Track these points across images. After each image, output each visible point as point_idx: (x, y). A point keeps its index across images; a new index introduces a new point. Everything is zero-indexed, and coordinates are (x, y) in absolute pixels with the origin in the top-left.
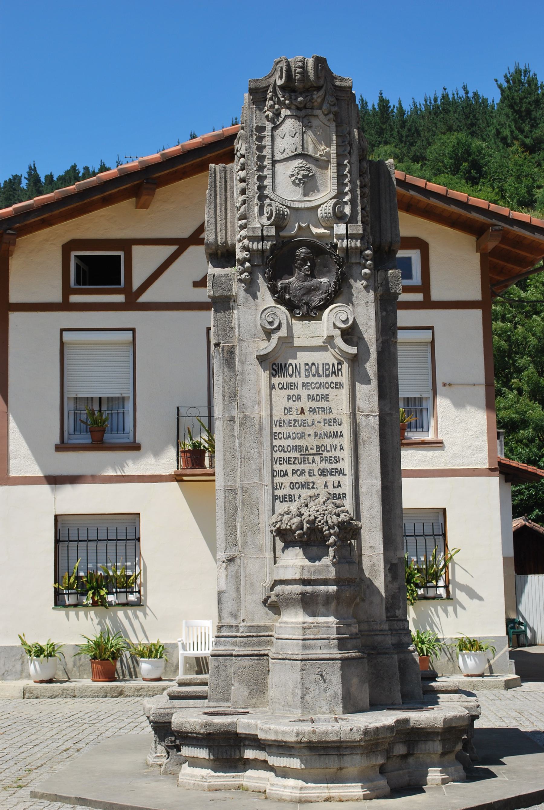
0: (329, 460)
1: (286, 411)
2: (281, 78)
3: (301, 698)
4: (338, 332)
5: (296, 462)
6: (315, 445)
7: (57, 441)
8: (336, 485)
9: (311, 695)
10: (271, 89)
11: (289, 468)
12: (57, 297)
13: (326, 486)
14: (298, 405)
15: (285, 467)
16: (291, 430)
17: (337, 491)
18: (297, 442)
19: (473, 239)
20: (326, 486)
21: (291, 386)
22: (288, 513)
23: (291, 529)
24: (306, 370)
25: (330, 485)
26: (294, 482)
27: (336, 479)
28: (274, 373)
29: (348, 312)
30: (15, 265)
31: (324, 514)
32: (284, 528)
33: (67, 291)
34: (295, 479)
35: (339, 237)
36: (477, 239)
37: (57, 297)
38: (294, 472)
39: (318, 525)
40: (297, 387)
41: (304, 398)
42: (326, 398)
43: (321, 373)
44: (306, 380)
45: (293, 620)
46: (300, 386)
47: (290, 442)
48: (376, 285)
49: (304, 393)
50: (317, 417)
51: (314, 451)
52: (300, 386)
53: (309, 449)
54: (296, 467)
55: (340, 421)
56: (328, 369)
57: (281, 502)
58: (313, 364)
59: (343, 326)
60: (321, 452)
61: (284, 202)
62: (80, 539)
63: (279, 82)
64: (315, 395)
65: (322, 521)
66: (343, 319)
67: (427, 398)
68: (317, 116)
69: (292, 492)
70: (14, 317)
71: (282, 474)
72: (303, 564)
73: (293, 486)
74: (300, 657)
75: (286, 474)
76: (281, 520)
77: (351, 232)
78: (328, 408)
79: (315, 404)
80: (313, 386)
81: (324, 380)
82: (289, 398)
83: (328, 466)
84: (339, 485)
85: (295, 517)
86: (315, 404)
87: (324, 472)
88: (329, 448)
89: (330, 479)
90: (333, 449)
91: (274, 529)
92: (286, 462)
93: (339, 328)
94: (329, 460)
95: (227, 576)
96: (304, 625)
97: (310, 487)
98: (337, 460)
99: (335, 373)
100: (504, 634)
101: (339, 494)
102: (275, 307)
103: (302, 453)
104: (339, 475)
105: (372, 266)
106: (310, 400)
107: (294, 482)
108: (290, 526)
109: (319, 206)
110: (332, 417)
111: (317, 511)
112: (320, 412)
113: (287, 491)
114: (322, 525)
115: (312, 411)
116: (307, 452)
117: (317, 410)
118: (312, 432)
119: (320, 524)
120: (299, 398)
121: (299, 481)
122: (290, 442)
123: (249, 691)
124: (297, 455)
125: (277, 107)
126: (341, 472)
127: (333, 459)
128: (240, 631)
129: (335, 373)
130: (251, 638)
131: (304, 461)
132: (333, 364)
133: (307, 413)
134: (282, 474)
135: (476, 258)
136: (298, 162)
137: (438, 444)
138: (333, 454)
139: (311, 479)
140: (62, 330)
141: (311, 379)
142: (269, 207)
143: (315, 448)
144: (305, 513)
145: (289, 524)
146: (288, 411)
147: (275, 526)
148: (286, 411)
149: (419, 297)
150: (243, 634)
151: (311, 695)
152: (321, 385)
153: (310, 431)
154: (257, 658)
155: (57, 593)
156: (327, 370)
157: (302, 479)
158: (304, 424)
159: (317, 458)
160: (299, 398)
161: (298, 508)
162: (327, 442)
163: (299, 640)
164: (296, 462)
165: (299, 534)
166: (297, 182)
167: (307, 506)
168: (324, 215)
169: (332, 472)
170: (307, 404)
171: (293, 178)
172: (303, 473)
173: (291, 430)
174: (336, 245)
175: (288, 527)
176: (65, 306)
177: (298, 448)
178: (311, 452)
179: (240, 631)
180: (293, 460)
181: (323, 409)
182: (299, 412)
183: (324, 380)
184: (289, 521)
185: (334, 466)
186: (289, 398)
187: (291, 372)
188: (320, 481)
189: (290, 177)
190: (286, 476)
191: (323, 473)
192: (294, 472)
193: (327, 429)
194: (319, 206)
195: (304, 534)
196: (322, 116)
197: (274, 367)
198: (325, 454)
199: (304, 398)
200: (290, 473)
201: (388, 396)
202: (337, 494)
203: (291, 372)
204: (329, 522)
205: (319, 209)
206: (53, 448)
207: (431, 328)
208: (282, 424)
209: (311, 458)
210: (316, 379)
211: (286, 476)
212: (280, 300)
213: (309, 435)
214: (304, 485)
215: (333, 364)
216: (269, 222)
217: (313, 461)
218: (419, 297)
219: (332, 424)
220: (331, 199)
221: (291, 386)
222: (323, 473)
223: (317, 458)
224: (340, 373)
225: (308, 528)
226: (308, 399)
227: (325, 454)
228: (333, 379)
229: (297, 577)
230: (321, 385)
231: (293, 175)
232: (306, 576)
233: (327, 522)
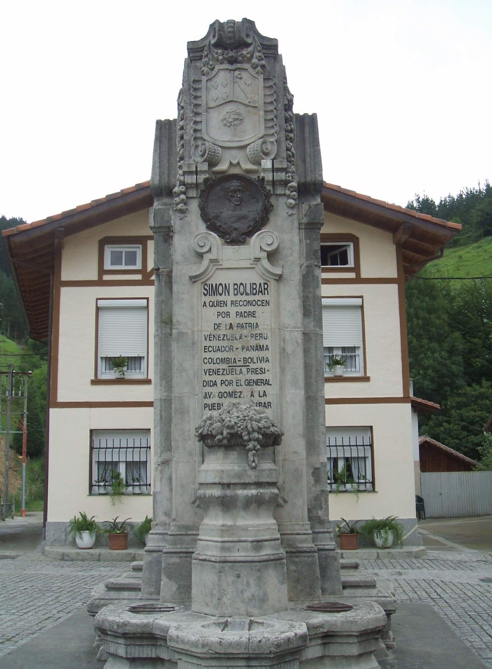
0: (255, 371)
1: (216, 327)
2: (214, 37)
3: (219, 599)
4: (265, 254)
5: (225, 373)
6: (242, 358)
7: (93, 378)
8: (261, 394)
9: (229, 596)
10: (206, 48)
11: (218, 379)
12: (95, 278)
13: (252, 395)
14: (228, 321)
15: (213, 378)
16: (221, 344)
17: (263, 400)
18: (225, 355)
19: (391, 235)
20: (252, 395)
21: (220, 304)
22: (210, 418)
23: (212, 435)
24: (235, 289)
25: (256, 394)
26: (223, 391)
27: (261, 388)
28: (206, 292)
29: (274, 237)
30: (66, 255)
31: (244, 420)
32: (206, 433)
33: (102, 271)
34: (224, 389)
35: (265, 170)
36: (394, 234)
37: (95, 278)
38: (223, 382)
39: (238, 431)
40: (226, 306)
41: (233, 314)
42: (253, 314)
43: (248, 291)
44: (235, 298)
45: (214, 523)
46: (229, 304)
47: (219, 355)
48: (301, 215)
49: (233, 310)
50: (245, 332)
51: (241, 363)
52: (229, 304)
53: (237, 361)
54: (224, 378)
55: (265, 336)
56: (255, 289)
57: (210, 410)
58: (242, 284)
59: (269, 249)
60: (247, 364)
61: (217, 142)
62: (135, 446)
63: (213, 42)
64: (243, 312)
65: (242, 427)
66: (269, 243)
67: (359, 347)
68: (247, 69)
69: (221, 401)
70: (65, 292)
71: (212, 384)
72: (219, 468)
73: (221, 395)
74: (218, 559)
75: (215, 384)
76: (204, 426)
77: (277, 167)
78: (255, 324)
79: (243, 320)
80: (241, 303)
81: (251, 298)
82: (219, 314)
83: (255, 377)
84: (265, 394)
85: (216, 423)
86: (243, 320)
87: (250, 382)
88: (255, 361)
89: (257, 389)
90: (259, 361)
91: (197, 434)
92: (215, 374)
93: (265, 251)
94: (255, 371)
95: (161, 478)
96: (223, 528)
97: (238, 396)
98: (263, 371)
99: (261, 292)
100: (415, 517)
101: (265, 403)
102: (207, 233)
103: (230, 365)
104: (264, 385)
105: (296, 197)
106: (238, 316)
107: (223, 391)
108: (211, 431)
109: (249, 144)
110: (258, 332)
111: (238, 417)
112: (248, 327)
113: (215, 400)
114: (242, 431)
115: (241, 326)
116: (235, 364)
117: (244, 325)
118: (240, 346)
119: (239, 429)
120: (228, 314)
121: (227, 391)
122: (219, 355)
123: (177, 586)
124: (225, 366)
125: (211, 63)
126: (267, 382)
127: (259, 370)
128: (171, 530)
129: (261, 292)
130: (180, 537)
131: (231, 372)
132: (260, 284)
133: (235, 328)
134: (212, 384)
135: (393, 249)
136: (228, 108)
137: (366, 379)
138: (259, 365)
139: (239, 389)
140: (97, 299)
141: (239, 298)
142: (203, 147)
143: (242, 360)
144: (226, 419)
145: (210, 430)
146: (217, 326)
147: (197, 432)
148: (216, 327)
149: (352, 275)
150: (173, 533)
151: (229, 596)
152: (249, 303)
153: (238, 344)
154: (185, 555)
155: (91, 486)
156: (253, 289)
157: (230, 389)
158: (233, 338)
159: (244, 369)
160: (228, 314)
161: (220, 415)
162: (254, 354)
163: (218, 542)
164: (225, 373)
165: (219, 439)
166: (228, 124)
167: (229, 412)
168: (252, 152)
169: (257, 382)
170: (234, 320)
171: (225, 122)
172: (230, 383)
173: (221, 344)
174: (263, 179)
175: (210, 433)
176: (100, 283)
177: (223, 361)
178: (239, 364)
179: (171, 530)
180: (221, 371)
181: (250, 325)
182: (228, 328)
183: (251, 298)
184: (209, 427)
185: (260, 377)
186: (219, 314)
187: (220, 292)
188: (246, 390)
189: (222, 121)
190: (215, 386)
191: (249, 383)
192: (223, 382)
193: (253, 342)
194: (249, 144)
195: (224, 438)
196: (251, 70)
197: (206, 287)
198: (252, 366)
199: (233, 314)
200: (219, 383)
201: (312, 314)
202: (263, 403)
203: (220, 292)
204: (249, 426)
205: (248, 147)
206: (90, 381)
207: (361, 297)
208: (212, 339)
209: (239, 368)
210: (244, 298)
211: (215, 386)
212: (212, 227)
213: (237, 349)
214: (230, 395)
215: (260, 284)
216: (202, 160)
217: (241, 372)
218: (352, 275)
219: (258, 338)
220: (259, 139)
221: (220, 304)
222: (249, 383)
223: (244, 369)
224: (266, 291)
225: (227, 433)
226: (237, 315)
227: (252, 366)
228: (260, 297)
229: (217, 480)
230: (249, 303)
231: (225, 119)
232: (225, 481)
233: (246, 427)
